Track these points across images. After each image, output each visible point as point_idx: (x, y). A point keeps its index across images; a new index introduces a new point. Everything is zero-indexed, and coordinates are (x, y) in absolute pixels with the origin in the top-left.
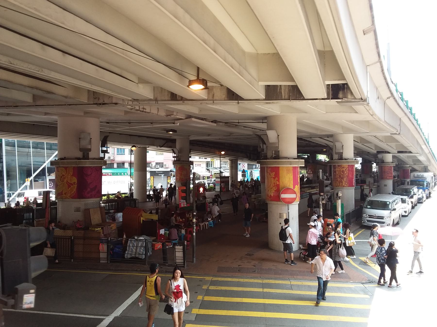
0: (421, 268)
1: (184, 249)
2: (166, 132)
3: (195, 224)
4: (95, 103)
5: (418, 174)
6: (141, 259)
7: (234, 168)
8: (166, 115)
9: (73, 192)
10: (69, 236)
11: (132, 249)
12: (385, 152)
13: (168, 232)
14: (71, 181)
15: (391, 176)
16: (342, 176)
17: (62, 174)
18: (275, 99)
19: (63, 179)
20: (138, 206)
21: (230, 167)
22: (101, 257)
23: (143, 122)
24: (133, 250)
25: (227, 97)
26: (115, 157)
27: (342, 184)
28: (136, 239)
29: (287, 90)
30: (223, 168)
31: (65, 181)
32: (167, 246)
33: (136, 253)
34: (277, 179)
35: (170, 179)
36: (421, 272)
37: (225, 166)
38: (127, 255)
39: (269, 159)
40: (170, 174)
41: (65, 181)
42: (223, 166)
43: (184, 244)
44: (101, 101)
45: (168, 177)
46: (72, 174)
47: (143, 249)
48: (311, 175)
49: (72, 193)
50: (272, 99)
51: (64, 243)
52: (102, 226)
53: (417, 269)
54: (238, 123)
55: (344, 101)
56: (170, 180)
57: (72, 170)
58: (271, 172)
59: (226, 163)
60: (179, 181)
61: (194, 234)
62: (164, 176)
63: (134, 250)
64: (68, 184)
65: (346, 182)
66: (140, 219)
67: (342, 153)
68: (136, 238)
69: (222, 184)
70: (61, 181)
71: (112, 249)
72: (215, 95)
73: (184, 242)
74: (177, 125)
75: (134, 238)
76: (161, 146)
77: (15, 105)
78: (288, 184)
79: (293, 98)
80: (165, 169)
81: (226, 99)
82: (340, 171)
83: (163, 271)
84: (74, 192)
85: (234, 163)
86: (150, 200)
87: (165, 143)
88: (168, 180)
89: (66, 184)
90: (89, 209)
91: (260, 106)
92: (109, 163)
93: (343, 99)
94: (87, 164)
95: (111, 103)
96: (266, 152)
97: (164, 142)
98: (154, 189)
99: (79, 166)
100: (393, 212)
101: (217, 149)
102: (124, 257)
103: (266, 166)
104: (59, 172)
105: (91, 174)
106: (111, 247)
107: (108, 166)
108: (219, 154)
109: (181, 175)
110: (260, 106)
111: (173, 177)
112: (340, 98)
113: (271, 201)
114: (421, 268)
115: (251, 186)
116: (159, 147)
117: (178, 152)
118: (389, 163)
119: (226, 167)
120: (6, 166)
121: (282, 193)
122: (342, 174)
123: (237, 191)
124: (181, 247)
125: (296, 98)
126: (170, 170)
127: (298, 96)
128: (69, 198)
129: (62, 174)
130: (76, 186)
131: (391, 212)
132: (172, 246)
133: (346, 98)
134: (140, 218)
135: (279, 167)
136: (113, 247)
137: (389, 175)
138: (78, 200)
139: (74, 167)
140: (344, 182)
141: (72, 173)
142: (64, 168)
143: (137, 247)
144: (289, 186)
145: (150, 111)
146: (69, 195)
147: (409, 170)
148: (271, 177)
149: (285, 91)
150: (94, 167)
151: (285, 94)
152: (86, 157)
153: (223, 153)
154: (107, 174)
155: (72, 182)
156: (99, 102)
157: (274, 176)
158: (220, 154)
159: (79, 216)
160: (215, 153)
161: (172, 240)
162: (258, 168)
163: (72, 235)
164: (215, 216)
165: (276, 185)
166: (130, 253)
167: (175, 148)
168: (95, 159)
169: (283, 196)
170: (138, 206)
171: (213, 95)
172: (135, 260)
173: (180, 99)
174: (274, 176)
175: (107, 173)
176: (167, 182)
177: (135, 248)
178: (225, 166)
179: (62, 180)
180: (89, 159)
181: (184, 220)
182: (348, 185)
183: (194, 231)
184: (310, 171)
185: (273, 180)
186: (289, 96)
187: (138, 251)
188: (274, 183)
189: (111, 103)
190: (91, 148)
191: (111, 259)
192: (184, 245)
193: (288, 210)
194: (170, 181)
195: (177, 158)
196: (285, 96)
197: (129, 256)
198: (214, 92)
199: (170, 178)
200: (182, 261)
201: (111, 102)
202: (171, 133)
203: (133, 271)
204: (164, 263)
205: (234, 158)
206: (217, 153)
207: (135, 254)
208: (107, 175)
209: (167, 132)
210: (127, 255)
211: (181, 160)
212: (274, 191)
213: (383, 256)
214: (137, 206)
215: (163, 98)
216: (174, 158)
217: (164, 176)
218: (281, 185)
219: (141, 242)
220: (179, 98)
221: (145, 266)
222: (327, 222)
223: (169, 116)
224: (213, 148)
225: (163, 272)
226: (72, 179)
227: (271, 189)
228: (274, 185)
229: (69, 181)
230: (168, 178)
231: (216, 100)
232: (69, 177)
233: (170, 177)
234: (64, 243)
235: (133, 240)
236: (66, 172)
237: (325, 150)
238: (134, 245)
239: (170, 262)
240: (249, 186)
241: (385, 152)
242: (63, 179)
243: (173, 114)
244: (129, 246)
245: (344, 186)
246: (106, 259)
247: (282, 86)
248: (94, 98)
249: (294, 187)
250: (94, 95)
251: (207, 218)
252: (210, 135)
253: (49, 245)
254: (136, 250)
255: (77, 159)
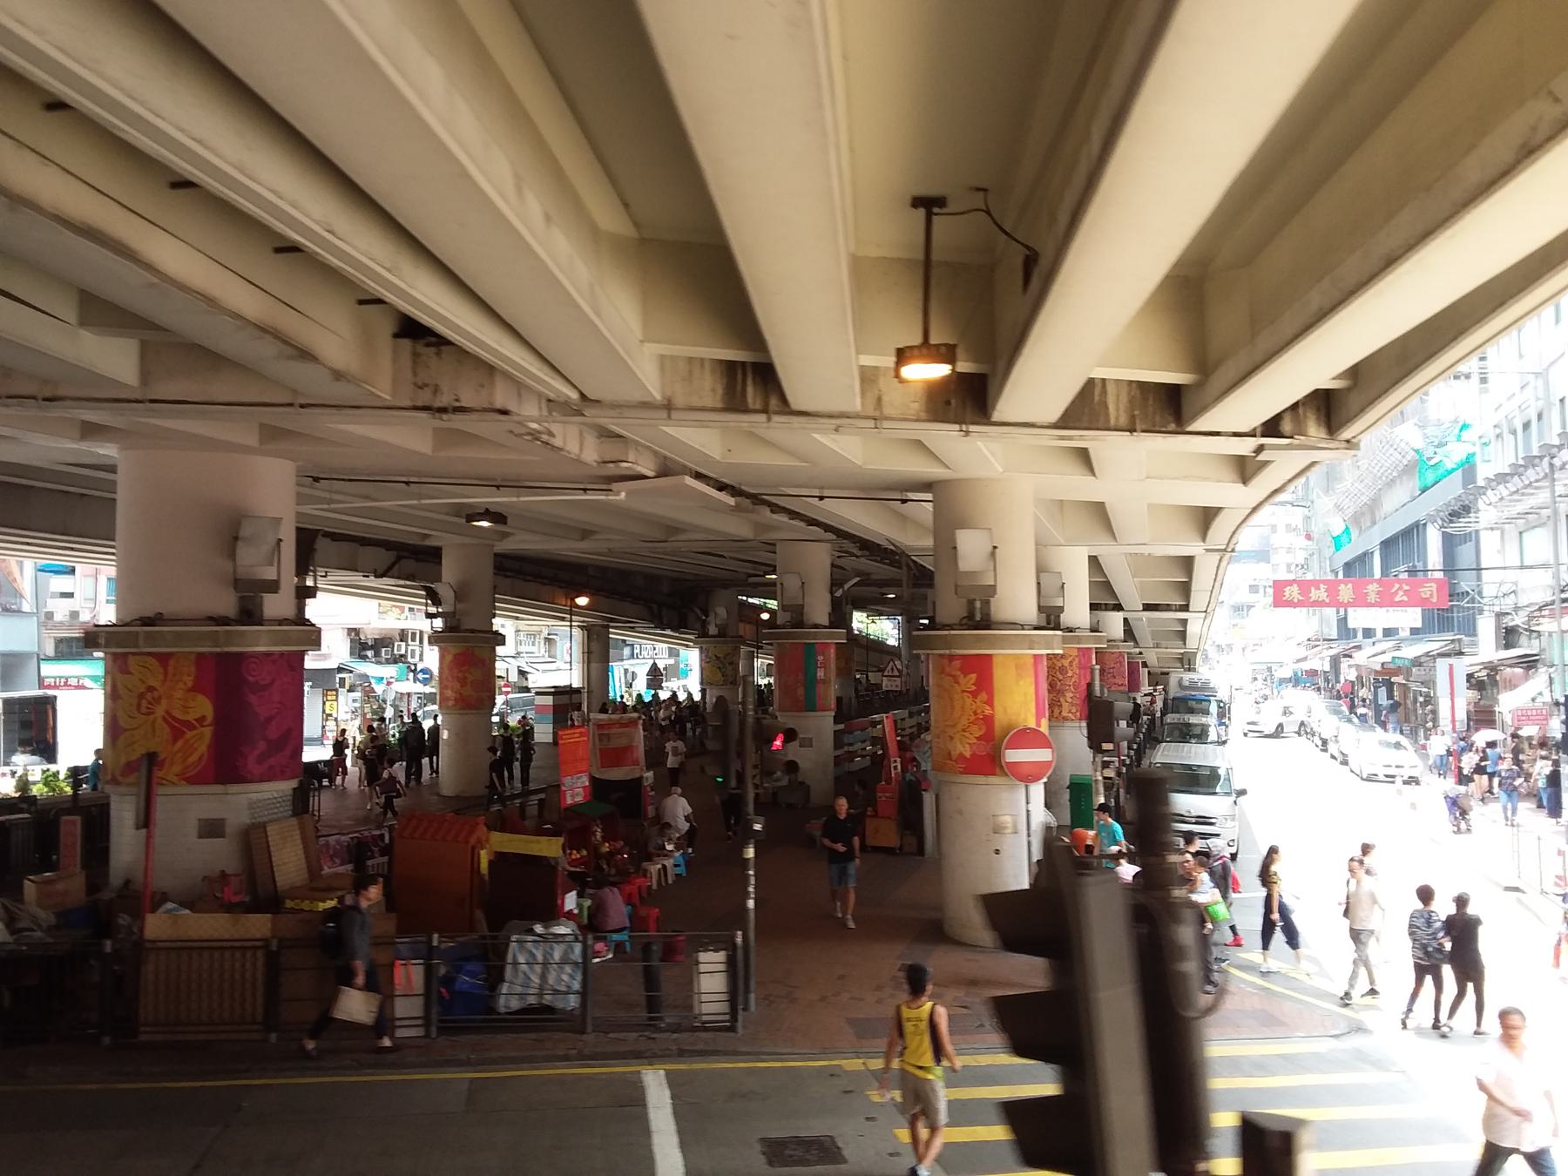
0: (1372, 982)
1: (731, 963)
2: (464, 521)
3: (752, 863)
4: (420, 404)
5: (1191, 677)
6: (563, 1011)
7: (598, 654)
8: (599, 460)
9: (194, 758)
10: (258, 936)
11: (525, 974)
12: (1103, 607)
13: (587, 903)
14: (188, 713)
15: (1122, 685)
16: (1059, 683)
17: (143, 682)
18: (1086, 425)
19: (150, 703)
20: (316, 808)
21: (583, 653)
22: (398, 1015)
23: (377, 478)
24: (533, 978)
25: (928, 411)
26: (99, 613)
27: (1061, 712)
28: (539, 935)
29: (1124, 399)
30: (524, 655)
31: (160, 711)
32: (595, 955)
33: (541, 988)
34: (983, 696)
35: (336, 700)
36: (1373, 992)
37: (531, 649)
38: (509, 999)
39: (954, 627)
40: (338, 680)
41: (160, 711)
42: (524, 651)
43: (734, 945)
44: (444, 400)
45: (329, 693)
46: (190, 684)
47: (570, 971)
48: (895, 681)
49: (191, 760)
50: (1077, 425)
51: (243, 966)
52: (340, 893)
53: (1363, 985)
54: (821, 498)
55: (1296, 445)
56: (335, 703)
57: (193, 669)
58: (963, 673)
59: (534, 638)
60: (454, 706)
61: (751, 904)
62: (311, 687)
63: (536, 980)
64: (173, 728)
65: (1072, 704)
66: (476, 855)
67: (803, 606)
68: (539, 929)
69: (576, 712)
70: (143, 714)
71: (448, 981)
72: (885, 399)
73: (733, 937)
74: (617, 498)
75: (531, 931)
76: (380, 571)
77: (48, 394)
78: (1022, 716)
79: (1144, 427)
80: (313, 660)
81: (923, 415)
82: (1054, 668)
83: (667, 1052)
84: (200, 758)
85: (595, 637)
86: (324, 784)
87: (393, 565)
88: (327, 703)
89: (166, 726)
90: (263, 826)
91: (351, 428)
92: (72, 638)
93: (1292, 437)
94: (258, 642)
95: (485, 410)
96: (1191, 610)
97: (386, 557)
98: (340, 739)
99: (226, 649)
100: (1241, 799)
101: (561, 587)
102: (492, 1010)
103: (947, 652)
104: (130, 673)
105: (273, 682)
106: (443, 971)
107: (65, 650)
108: (565, 606)
109: (463, 682)
110: (351, 428)
111: (348, 691)
112: (1288, 435)
113: (962, 773)
114: (1372, 982)
115: (668, 722)
116: (373, 578)
117: (456, 597)
118: (1114, 641)
119: (532, 653)
120: (276, 645)
121: (1006, 749)
122: (1061, 678)
123: (675, 744)
124: (720, 956)
125: (1154, 426)
126: (336, 666)
127: (1158, 418)
128: (175, 782)
129: (143, 682)
130: (207, 732)
131: (1235, 802)
132: (610, 956)
133: (1302, 435)
134: (476, 850)
135: (990, 656)
136: (448, 972)
137: (1117, 681)
138: (218, 788)
139: (200, 656)
140: (1065, 706)
141: (190, 681)
142: (153, 657)
143: (546, 964)
144: (1025, 720)
145: (565, 443)
146: (177, 769)
147: (1138, 663)
148: (964, 691)
149: (1118, 400)
150: (282, 654)
151: (1118, 410)
152: (249, 614)
153: (582, 601)
154: (63, 680)
155: (191, 717)
156: (437, 404)
157: (974, 688)
158: (571, 606)
159: (220, 855)
160: (556, 601)
161: (610, 932)
162: (639, 656)
163: (268, 934)
164: (677, 835)
165: (981, 717)
166: (519, 989)
167: (439, 580)
168: (286, 622)
169: (1013, 756)
170: (316, 808)
171: (879, 400)
172: (539, 1017)
173: (758, 406)
174: (974, 688)
175: (60, 677)
176: (324, 711)
177: (538, 968)
178: (531, 649)
179: (149, 708)
180: (993, 627)
181: (584, 853)
182: (1078, 714)
183: (748, 893)
184: (892, 669)
185: (969, 701)
186: (1133, 417)
187: (551, 979)
188: (975, 713)
189: (485, 410)
190: (995, 581)
191: (441, 1021)
192: (731, 947)
193: (1027, 803)
194: (335, 706)
195: (449, 619)
196: (1117, 418)
197: (515, 1004)
198: (880, 390)
199: (337, 696)
200: (723, 1007)
201: (486, 405)
202: (485, 524)
203: (551, 1059)
204: (651, 1019)
205: (599, 622)
206: (559, 602)
207: (540, 995)
208: (62, 684)
209: (467, 522)
210: (509, 999)
211: (466, 626)
212: (975, 741)
213: (1435, 938)
214: (313, 810)
215: (696, 402)
216: (430, 620)
217: (311, 687)
218: (1001, 718)
219: (561, 945)
220: (754, 403)
221: (584, 1037)
222: (1085, 841)
223: (611, 465)
224: (530, 578)
225: (669, 1056)
226: (192, 704)
227: (964, 730)
228: (973, 718)
229: (178, 714)
230: (329, 698)
231: (887, 418)
232: (179, 694)
233: (334, 693)
234: (243, 966)
235: (530, 938)
236: (161, 677)
237: (893, 596)
238: (533, 955)
239: (669, 1018)
240: (663, 723)
241: (1103, 607)
242: (150, 703)
243: (624, 459)
244: (516, 963)
245: (1065, 719)
246: (419, 1022)
247: (1107, 382)
248: (415, 384)
249: (1038, 724)
250: (415, 374)
251: (660, 842)
252: (592, 533)
253: (360, 980)
254: (543, 977)
255: (213, 623)
